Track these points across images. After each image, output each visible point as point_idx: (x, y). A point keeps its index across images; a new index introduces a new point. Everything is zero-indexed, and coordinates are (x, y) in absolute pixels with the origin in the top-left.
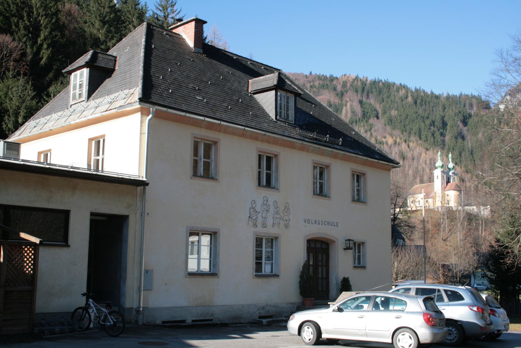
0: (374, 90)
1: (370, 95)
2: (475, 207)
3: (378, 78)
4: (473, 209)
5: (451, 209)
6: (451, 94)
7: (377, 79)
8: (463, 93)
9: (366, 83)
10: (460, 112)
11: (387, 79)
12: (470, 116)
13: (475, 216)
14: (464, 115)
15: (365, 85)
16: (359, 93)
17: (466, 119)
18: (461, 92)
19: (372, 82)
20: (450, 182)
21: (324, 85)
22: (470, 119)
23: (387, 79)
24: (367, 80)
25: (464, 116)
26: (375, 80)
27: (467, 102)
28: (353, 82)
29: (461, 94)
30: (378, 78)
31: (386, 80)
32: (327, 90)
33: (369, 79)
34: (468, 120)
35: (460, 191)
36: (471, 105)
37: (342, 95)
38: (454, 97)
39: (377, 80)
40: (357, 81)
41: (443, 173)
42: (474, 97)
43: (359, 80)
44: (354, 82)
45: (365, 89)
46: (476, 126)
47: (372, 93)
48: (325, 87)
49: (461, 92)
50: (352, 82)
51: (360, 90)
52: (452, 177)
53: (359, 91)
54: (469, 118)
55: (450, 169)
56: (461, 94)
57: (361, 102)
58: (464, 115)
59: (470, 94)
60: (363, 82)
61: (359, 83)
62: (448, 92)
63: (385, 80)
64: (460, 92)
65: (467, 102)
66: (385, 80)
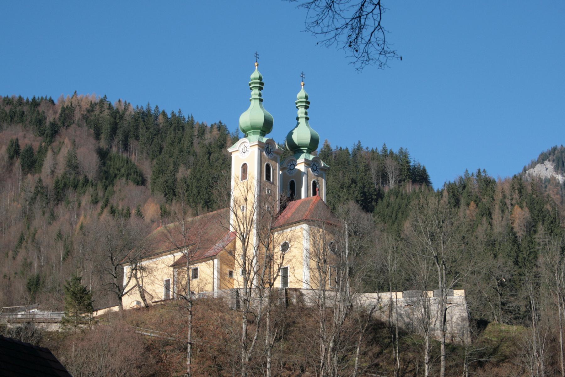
0: (142, 131)
1: (133, 143)
2: (400, 294)
3: (157, 107)
4: (391, 304)
5: (294, 301)
6: (333, 148)
7: (153, 109)
8: (364, 146)
9: (123, 114)
10: (354, 181)
11: (180, 112)
12: (380, 195)
13: (403, 333)
14: (366, 190)
15: (121, 117)
16: (103, 136)
17: (370, 202)
18: (359, 142)
19: (139, 113)
20: (300, 197)
21: (15, 113)
22: (380, 201)
23: (180, 112)
24: (126, 109)
25: (364, 194)
26: (149, 110)
27: (374, 166)
28: (91, 110)
29: (359, 148)
30: (157, 107)
31: (177, 114)
32: (20, 125)
33: (133, 107)
34: (374, 203)
35: (331, 227)
36: (384, 177)
37: (54, 131)
38: (343, 152)
39: (153, 112)
40: (102, 107)
41: (268, 153)
42: (387, 154)
43: (106, 106)
44: (93, 111)
45: (119, 126)
46: (393, 216)
47: (137, 138)
48: (15, 119)
49: (359, 142)
50: (88, 111)
51: (106, 130)
52: (304, 178)
53: (103, 131)
54: (376, 200)
55: (296, 149)
56: (359, 148)
57: (103, 155)
58: (366, 190)
59: (380, 149)
60: (117, 111)
61: (106, 112)
62: (326, 141)
63: (173, 114)
64: (357, 143)
65: (374, 166)
66: (173, 114)
